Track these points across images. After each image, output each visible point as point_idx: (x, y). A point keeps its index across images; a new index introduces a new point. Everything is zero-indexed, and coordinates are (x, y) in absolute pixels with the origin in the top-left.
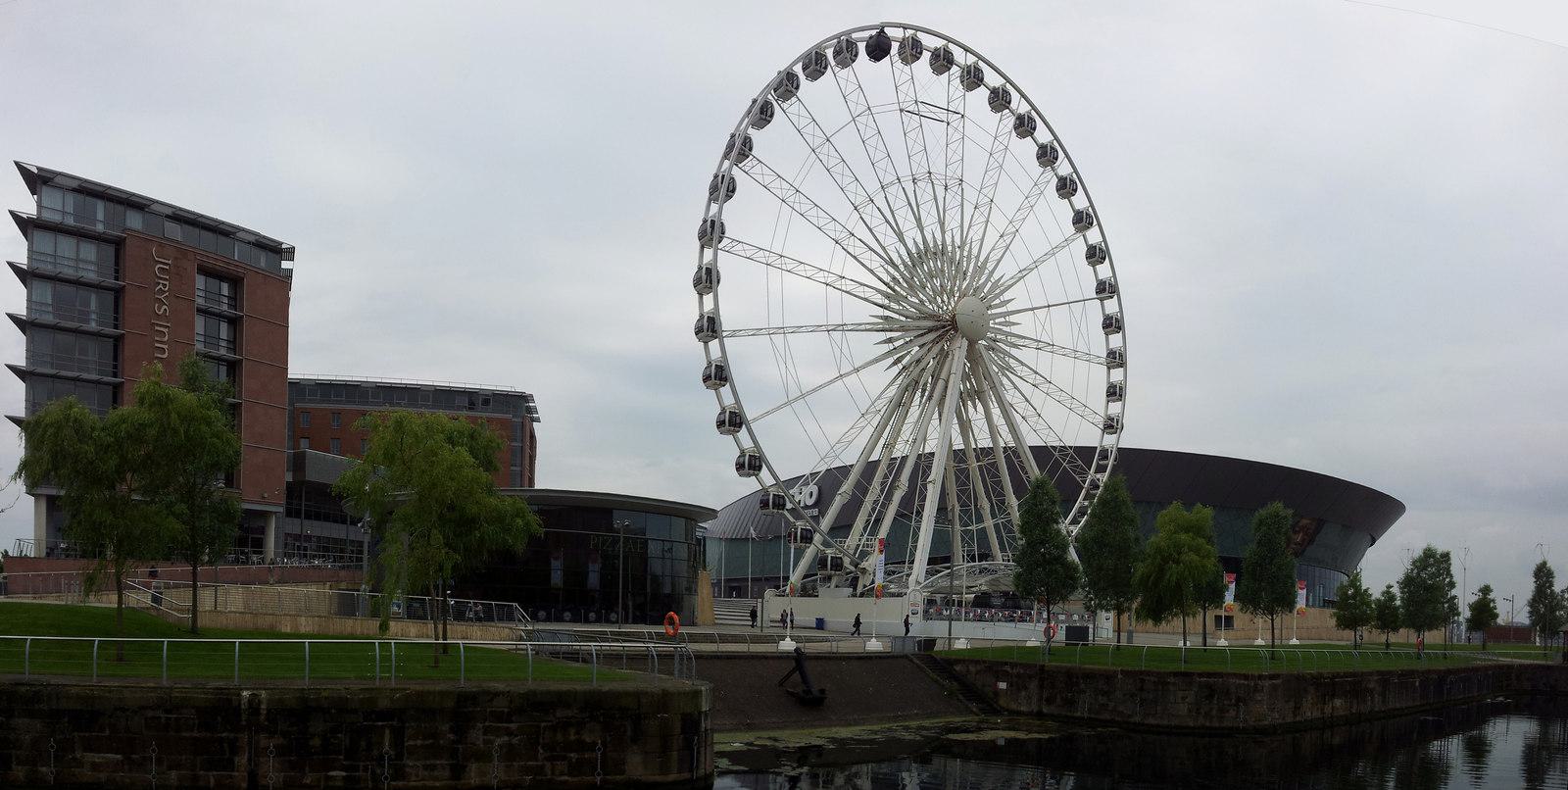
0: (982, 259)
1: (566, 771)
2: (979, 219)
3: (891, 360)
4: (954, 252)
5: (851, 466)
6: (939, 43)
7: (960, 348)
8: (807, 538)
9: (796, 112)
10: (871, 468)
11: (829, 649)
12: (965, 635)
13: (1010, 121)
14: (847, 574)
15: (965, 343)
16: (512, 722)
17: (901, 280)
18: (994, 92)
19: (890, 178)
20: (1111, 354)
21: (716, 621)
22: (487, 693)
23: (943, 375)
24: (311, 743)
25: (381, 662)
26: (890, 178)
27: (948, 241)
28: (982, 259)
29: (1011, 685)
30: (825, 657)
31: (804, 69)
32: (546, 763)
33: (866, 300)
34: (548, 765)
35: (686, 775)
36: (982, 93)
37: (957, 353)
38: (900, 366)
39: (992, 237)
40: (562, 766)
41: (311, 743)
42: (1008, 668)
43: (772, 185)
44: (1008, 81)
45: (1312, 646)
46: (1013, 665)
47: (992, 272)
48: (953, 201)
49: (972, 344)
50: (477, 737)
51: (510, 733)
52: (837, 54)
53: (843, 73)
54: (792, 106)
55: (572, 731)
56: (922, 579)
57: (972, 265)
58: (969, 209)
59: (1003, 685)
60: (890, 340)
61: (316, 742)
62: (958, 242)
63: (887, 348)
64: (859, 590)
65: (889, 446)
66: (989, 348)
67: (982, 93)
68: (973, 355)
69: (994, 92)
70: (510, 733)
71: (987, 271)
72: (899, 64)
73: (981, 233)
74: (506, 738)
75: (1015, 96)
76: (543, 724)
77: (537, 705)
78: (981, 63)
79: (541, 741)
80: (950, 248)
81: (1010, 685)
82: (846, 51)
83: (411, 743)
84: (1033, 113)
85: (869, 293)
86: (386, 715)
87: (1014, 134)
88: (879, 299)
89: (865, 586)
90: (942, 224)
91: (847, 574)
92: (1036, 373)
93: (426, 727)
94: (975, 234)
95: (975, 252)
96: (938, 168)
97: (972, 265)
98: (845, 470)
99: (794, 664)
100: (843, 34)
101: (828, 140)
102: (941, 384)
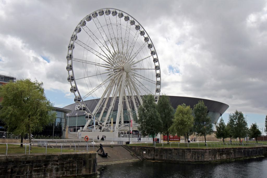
0: (131, 57)
1: (69, 173)
2: (131, 49)
3: (108, 74)
4: (125, 54)
5: (100, 99)
6: (126, 15)
7: (124, 74)
8: (90, 117)
9: (96, 22)
10: (104, 99)
11: (104, 144)
12: (134, 141)
13: (139, 32)
14: (99, 126)
15: (126, 73)
16: (58, 162)
17: (111, 58)
18: (126, 17)
19: (113, 37)
20: (158, 82)
21: (69, 138)
22: (53, 155)
23: (121, 80)
24: (8, 171)
25: (27, 148)
26: (113, 37)
27: (124, 52)
28: (131, 57)
29: (147, 152)
30: (35, 148)
31: (99, 13)
32: (65, 172)
33: (104, 60)
34: (65, 172)
35: (94, 173)
36: (129, 22)
37: (124, 75)
38: (110, 76)
39: (133, 53)
40: (69, 172)
41: (8, 171)
42: (146, 148)
43: (95, 39)
44: (134, 19)
45: (210, 142)
46: (147, 148)
47: (132, 60)
48: (126, 45)
49: (127, 73)
50: (50, 166)
51: (57, 165)
52: (106, 12)
53: (106, 16)
54: (95, 19)
55: (71, 164)
56: (118, 127)
57: (128, 58)
58: (129, 47)
59: (145, 152)
60: (109, 70)
61: (10, 170)
62: (126, 52)
63: (107, 71)
64: (102, 130)
65: (108, 96)
66: (133, 75)
67: (129, 22)
68: (127, 76)
69: (126, 17)
70: (57, 165)
71: (131, 59)
72: (118, 17)
73: (131, 52)
74: (56, 166)
75: (141, 27)
76: (65, 162)
77: (64, 158)
78: (134, 20)
79: (64, 166)
80: (124, 53)
81: (146, 152)
82: (108, 12)
83: (35, 169)
84: (144, 31)
85: (137, 76)
86: (28, 162)
87: (140, 34)
88: (136, 75)
89: (103, 129)
90: (123, 48)
91: (99, 126)
92: (140, 83)
93: (38, 165)
94: (130, 51)
95: (129, 55)
96: (123, 37)
97: (128, 58)
98: (98, 100)
99: (100, 147)
100: (108, 8)
101: (102, 27)
102: (120, 82)
